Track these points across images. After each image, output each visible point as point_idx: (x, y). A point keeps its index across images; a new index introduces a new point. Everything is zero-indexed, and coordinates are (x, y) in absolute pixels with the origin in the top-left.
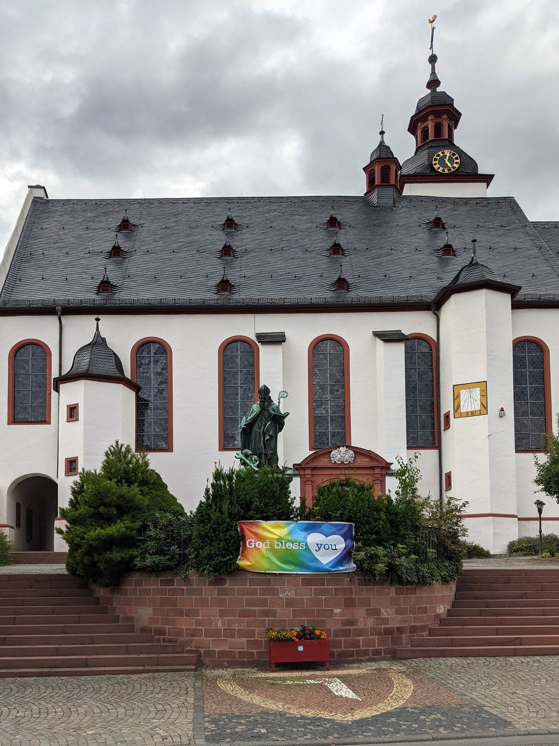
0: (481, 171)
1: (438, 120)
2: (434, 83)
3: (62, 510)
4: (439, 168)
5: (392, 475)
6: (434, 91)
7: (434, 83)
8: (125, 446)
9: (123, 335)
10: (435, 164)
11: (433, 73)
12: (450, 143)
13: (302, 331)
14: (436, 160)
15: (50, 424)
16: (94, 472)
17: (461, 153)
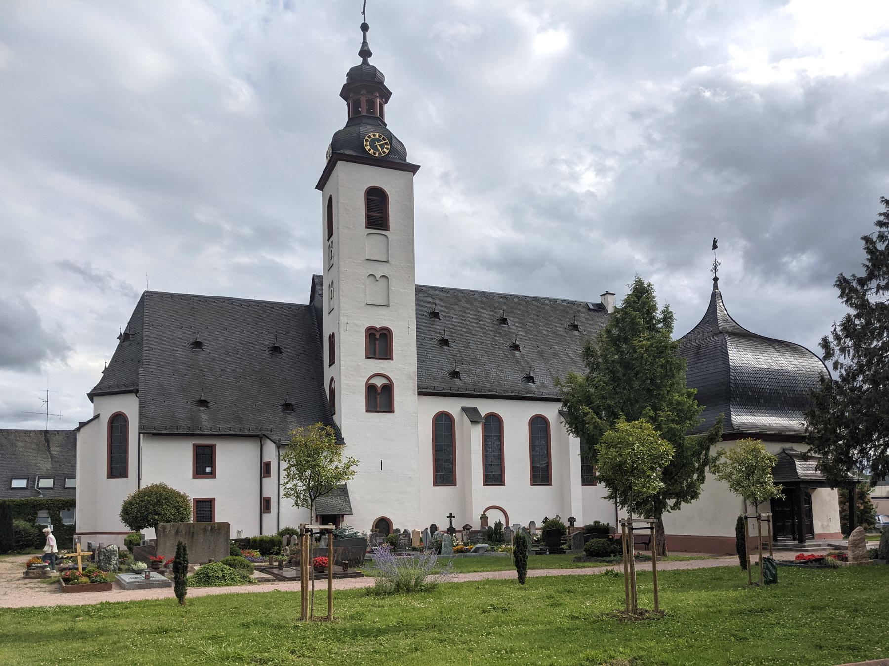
0: (409, 160)
2: (365, 53)
3: (855, 316)
5: (660, 527)
6: (365, 62)
7: (365, 53)
8: (831, 338)
9: (485, 407)
11: (365, 43)
12: (379, 122)
13: (527, 411)
14: (367, 141)
15: (532, 485)
16: (567, 524)
17: (390, 136)
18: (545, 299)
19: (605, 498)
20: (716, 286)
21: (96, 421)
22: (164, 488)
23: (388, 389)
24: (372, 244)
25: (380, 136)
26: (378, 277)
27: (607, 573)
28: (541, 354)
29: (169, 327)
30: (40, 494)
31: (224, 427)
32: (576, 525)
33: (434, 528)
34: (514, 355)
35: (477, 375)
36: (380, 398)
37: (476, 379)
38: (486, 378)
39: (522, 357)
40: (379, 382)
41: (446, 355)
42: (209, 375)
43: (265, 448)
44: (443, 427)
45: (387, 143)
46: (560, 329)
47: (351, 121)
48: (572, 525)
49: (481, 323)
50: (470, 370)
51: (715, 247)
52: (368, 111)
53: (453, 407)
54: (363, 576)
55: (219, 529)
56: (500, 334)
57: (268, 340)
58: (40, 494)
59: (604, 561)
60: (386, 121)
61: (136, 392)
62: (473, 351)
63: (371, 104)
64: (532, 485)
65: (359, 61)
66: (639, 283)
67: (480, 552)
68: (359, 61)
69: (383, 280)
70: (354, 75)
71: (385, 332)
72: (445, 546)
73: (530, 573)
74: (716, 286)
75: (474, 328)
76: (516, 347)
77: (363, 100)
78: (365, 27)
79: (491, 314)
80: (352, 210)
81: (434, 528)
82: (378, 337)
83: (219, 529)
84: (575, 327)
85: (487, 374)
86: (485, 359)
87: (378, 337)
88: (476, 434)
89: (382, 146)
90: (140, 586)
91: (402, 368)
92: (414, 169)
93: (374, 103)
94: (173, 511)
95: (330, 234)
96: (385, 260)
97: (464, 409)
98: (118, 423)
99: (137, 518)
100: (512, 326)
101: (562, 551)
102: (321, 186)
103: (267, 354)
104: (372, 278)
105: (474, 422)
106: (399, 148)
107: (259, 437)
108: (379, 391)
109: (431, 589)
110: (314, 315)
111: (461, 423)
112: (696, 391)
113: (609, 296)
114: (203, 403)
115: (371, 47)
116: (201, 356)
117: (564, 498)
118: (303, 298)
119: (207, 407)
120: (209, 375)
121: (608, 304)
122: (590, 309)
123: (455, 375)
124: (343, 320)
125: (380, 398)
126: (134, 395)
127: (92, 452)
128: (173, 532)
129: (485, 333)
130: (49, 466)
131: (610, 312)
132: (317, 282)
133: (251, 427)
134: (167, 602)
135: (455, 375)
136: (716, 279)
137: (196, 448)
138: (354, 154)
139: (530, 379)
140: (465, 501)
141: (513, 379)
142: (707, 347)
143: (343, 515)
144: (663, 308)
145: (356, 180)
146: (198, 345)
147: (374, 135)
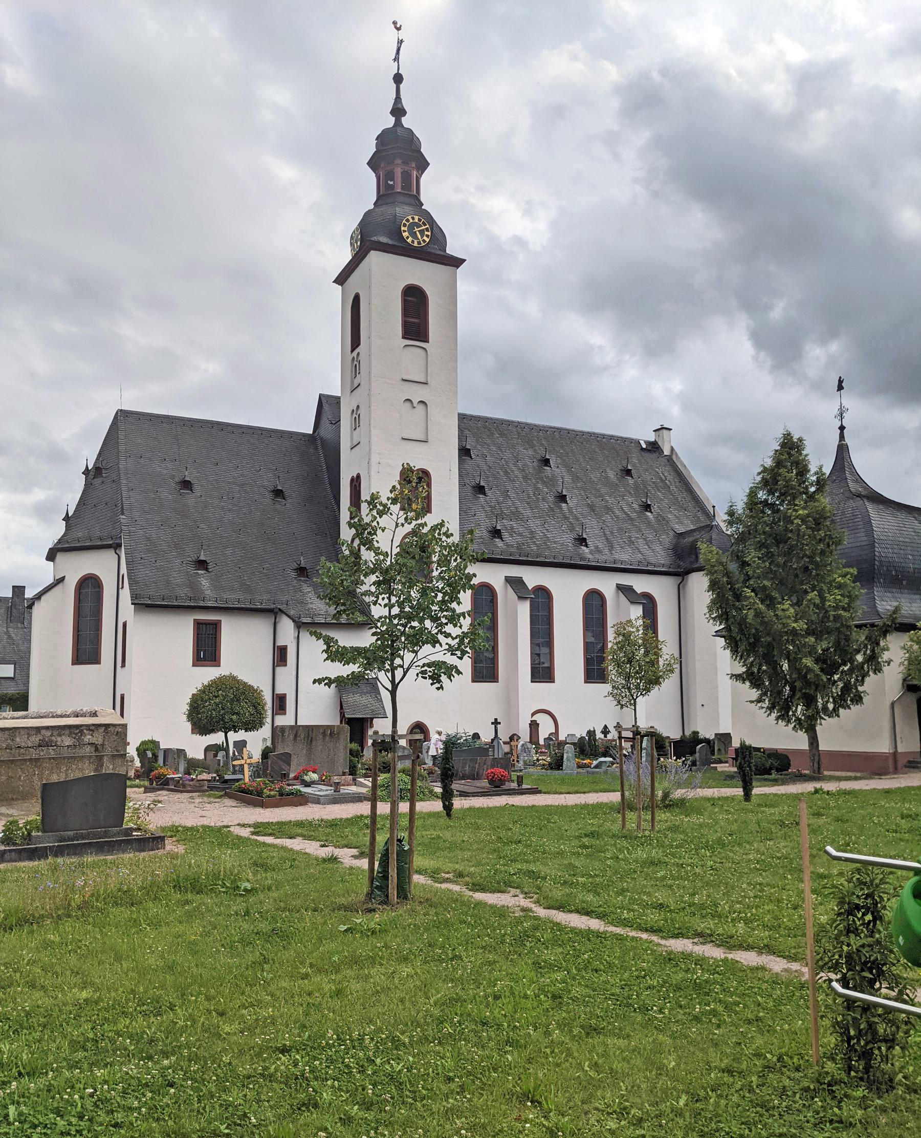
1: (406, 168)
2: (398, 111)
6: (398, 123)
7: (398, 111)
9: (533, 577)
10: (404, 231)
11: (398, 99)
14: (405, 225)
18: (591, 434)
19: (752, 702)
20: (842, 437)
21: (60, 586)
22: (234, 678)
24: (410, 359)
25: (420, 220)
26: (415, 402)
27: (817, 791)
28: (591, 507)
29: (150, 459)
31: (233, 598)
33: (476, 736)
34: (560, 508)
35: (521, 535)
37: (519, 539)
38: (531, 538)
39: (570, 510)
41: (483, 507)
42: (202, 526)
45: (427, 230)
46: (611, 474)
47: (381, 199)
49: (520, 464)
50: (512, 528)
51: (840, 387)
52: (403, 188)
54: (540, 792)
55: (338, 733)
56: (541, 479)
57: (268, 480)
59: (765, 780)
60: (422, 200)
61: (116, 547)
62: (514, 503)
63: (406, 176)
65: (390, 122)
66: (788, 436)
67: (604, 768)
68: (390, 122)
69: (421, 408)
70: (383, 138)
72: (568, 760)
73: (756, 791)
74: (842, 437)
75: (512, 471)
76: (562, 498)
77: (398, 172)
78: (398, 79)
79: (530, 452)
81: (476, 736)
83: (338, 733)
84: (628, 472)
85: (532, 533)
86: (528, 513)
88: (524, 610)
89: (422, 232)
90: (334, 801)
92: (456, 262)
93: (410, 175)
94: (251, 709)
95: (356, 342)
96: (423, 380)
98: (89, 588)
99: (212, 718)
100: (556, 469)
102: (342, 279)
103: (269, 496)
104: (408, 404)
105: (521, 598)
106: (439, 236)
107: (273, 613)
109: (681, 803)
112: (854, 571)
113: (664, 431)
114: (202, 564)
115: (406, 104)
116: (191, 499)
118: (303, 422)
119: (207, 569)
120: (202, 526)
121: (664, 442)
122: (642, 449)
123: (496, 533)
124: (375, 458)
126: (112, 551)
127: (51, 629)
128: (292, 737)
129: (525, 478)
131: (666, 453)
132: (327, 407)
133: (262, 599)
134: (436, 815)
135: (496, 533)
136: (842, 428)
137: (198, 624)
139: (582, 541)
140: (510, 701)
141: (561, 541)
142: (843, 513)
143: (372, 719)
144: (816, 469)
145: (389, 274)
146: (186, 484)
147: (413, 218)
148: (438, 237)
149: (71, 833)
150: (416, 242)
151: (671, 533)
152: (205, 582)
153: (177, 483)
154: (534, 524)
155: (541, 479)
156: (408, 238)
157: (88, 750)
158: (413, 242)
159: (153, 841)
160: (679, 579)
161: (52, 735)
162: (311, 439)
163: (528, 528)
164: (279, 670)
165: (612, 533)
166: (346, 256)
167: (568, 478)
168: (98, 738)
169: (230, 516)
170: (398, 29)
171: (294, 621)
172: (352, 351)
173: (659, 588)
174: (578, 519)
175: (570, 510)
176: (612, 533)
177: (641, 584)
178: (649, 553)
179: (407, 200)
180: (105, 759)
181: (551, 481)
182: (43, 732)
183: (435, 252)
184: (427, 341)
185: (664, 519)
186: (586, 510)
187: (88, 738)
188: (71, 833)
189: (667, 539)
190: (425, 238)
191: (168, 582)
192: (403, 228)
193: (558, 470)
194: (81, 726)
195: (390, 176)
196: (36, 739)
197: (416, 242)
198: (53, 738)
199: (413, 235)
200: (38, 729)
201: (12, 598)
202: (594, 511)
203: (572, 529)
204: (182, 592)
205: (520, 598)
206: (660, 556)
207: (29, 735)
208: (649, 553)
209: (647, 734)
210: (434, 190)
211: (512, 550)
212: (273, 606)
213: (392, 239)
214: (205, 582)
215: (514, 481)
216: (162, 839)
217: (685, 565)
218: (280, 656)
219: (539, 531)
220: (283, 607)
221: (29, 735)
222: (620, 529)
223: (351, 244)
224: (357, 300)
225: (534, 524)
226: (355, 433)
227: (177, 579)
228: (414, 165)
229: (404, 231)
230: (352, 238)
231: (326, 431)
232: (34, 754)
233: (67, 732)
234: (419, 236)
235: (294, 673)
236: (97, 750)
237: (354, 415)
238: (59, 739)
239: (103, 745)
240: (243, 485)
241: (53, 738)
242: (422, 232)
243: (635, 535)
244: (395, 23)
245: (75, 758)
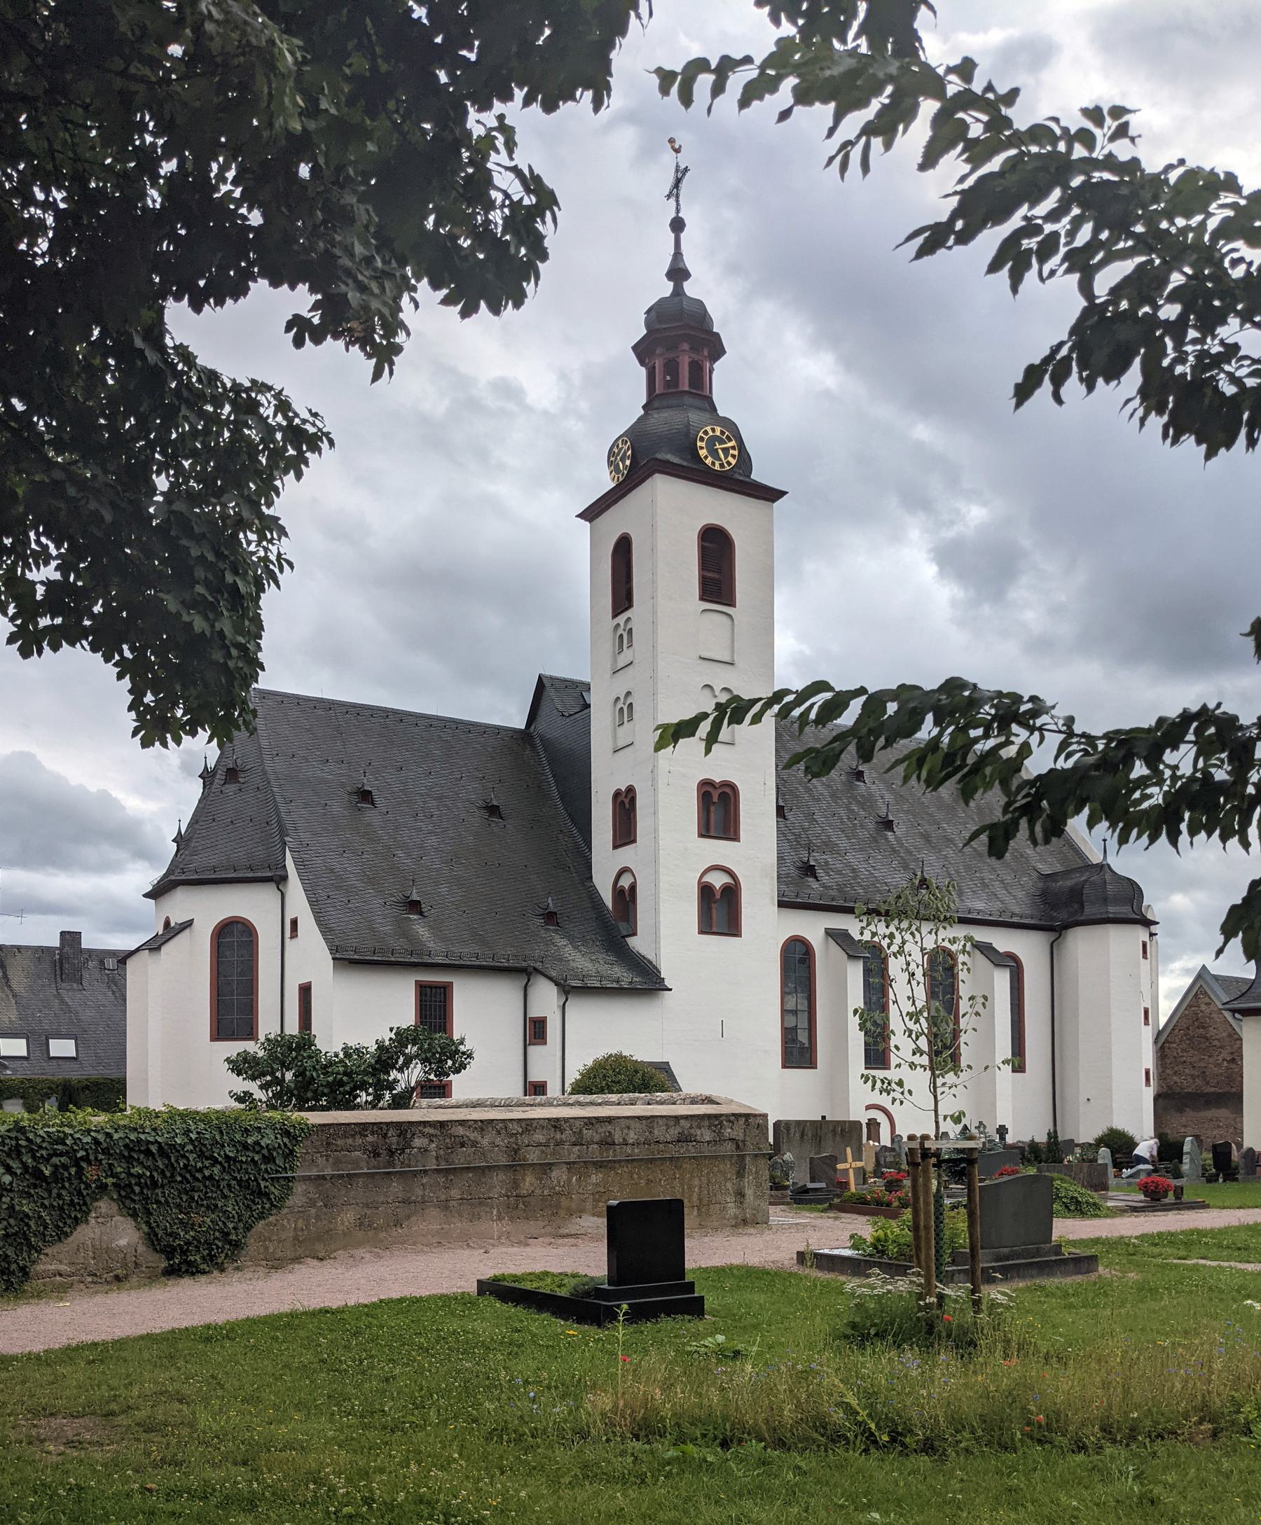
1: (696, 357)
2: (678, 273)
4: (706, 457)
6: (678, 292)
7: (678, 273)
10: (702, 448)
11: (678, 254)
14: (702, 439)
15: (784, 1067)
21: (187, 932)
23: (731, 893)
28: (926, 837)
30: (6, 1067)
31: (468, 952)
32: (1010, 1139)
35: (839, 872)
36: (720, 908)
40: (718, 880)
43: (531, 991)
44: (797, 963)
45: (733, 448)
48: (1002, 1138)
50: (827, 863)
53: (813, 928)
55: (850, 1132)
56: (855, 798)
58: (6, 1067)
64: (784, 1067)
65: (667, 288)
68: (667, 288)
71: (728, 790)
76: (888, 825)
78: (678, 225)
80: (670, 568)
82: (715, 799)
83: (850, 1132)
85: (854, 870)
87: (715, 799)
88: (855, 974)
89: (726, 451)
91: (755, 856)
92: (771, 495)
96: (727, 659)
97: (830, 933)
101: (1237, 1180)
102: (591, 514)
104: (707, 691)
107: (523, 972)
108: (718, 896)
110: (540, 748)
111: (826, 957)
114: (414, 906)
115: (690, 262)
116: (372, 816)
117: (837, 1087)
119: (421, 913)
125: (720, 908)
126: (273, 885)
129: (834, 796)
130: (13, 1015)
133: (506, 954)
137: (422, 988)
138: (676, 460)
145: (673, 514)
146: (365, 796)
147: (713, 430)
148: (745, 460)
149: (1006, 1250)
150: (717, 463)
151: (1035, 875)
152: (421, 930)
153: (350, 794)
154: (854, 858)
155: (855, 798)
156: (706, 457)
157: (729, 1146)
158: (713, 464)
159: (1083, 1263)
160: (1052, 936)
161: (691, 1127)
162: (524, 737)
163: (848, 865)
164: (532, 1050)
165: (957, 872)
166: (606, 482)
167: (889, 797)
168: (737, 1132)
169: (433, 841)
170: (677, 151)
171: (557, 984)
172: (615, 616)
173: (1027, 947)
174: (910, 853)
175: (898, 839)
176: (957, 872)
177: (1003, 941)
178: (1008, 899)
179: (697, 402)
180: (748, 1159)
181: (867, 802)
182: (682, 1122)
183: (739, 481)
184: (732, 604)
185: (1022, 856)
186: (920, 842)
187: (728, 1132)
188: (1006, 1250)
189: (1029, 882)
190: (730, 459)
191: (372, 929)
192: (699, 444)
193: (873, 787)
194: (721, 1115)
195: (672, 367)
196: (674, 1132)
197: (717, 463)
198: (692, 1131)
199: (713, 453)
200: (677, 1118)
201: (61, 948)
202: (929, 842)
203: (906, 867)
204: (398, 944)
205: (850, 957)
206: (1018, 902)
207: (668, 1127)
208: (1008, 899)
209: (1101, 1142)
210: (729, 387)
211: (832, 893)
212: (524, 964)
213: (683, 459)
214: (421, 930)
215: (819, 800)
216: (1093, 1259)
217: (1063, 915)
218: (535, 1031)
219: (862, 867)
220: (538, 965)
221: (668, 1127)
222: (968, 868)
223: (610, 463)
224: (623, 548)
225: (854, 858)
226: (621, 731)
227: (385, 928)
228: (706, 353)
229: (702, 448)
230: (611, 453)
231: (549, 725)
232: (673, 1151)
233: (706, 1123)
234: (722, 456)
235: (559, 1054)
236: (738, 1147)
237: (620, 705)
238: (699, 1132)
239: (744, 1141)
240: (440, 798)
241: (692, 1131)
242: (726, 451)
243: (988, 876)
244: (671, 141)
245: (716, 1157)
